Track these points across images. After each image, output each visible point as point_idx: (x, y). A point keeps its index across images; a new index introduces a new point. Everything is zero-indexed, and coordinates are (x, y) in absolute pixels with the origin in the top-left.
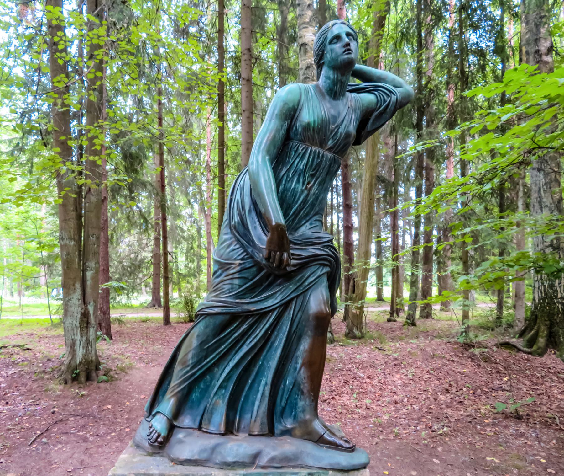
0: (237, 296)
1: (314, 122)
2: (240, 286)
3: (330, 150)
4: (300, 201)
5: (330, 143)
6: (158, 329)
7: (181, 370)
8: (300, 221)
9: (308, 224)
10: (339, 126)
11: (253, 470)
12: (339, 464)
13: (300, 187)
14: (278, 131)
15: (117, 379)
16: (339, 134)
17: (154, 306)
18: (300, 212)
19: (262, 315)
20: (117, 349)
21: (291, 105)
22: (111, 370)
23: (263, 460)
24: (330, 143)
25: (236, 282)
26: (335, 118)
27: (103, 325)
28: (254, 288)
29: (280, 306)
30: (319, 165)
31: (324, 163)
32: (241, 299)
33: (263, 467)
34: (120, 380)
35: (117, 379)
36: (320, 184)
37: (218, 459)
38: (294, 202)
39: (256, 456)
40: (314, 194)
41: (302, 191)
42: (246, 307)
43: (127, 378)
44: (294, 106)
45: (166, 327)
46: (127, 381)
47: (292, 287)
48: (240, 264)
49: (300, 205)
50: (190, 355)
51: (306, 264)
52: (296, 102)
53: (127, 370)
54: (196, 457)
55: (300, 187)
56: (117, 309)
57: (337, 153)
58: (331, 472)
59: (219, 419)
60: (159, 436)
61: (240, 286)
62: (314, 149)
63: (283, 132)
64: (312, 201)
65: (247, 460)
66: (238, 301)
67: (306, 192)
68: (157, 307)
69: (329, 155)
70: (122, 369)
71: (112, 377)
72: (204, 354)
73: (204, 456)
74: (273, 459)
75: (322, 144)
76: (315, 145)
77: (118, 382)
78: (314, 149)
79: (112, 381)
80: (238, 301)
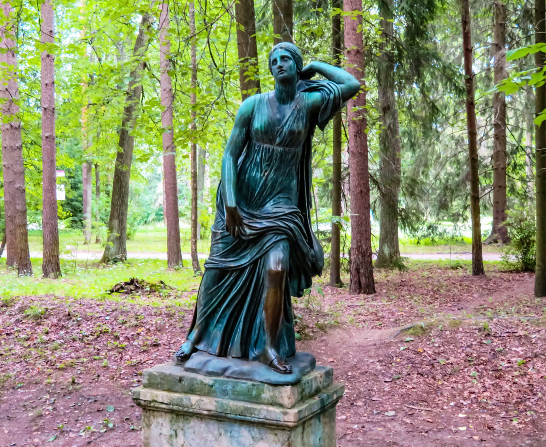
0: (222, 256)
1: (261, 127)
2: (224, 249)
3: (279, 145)
4: (260, 185)
5: (278, 140)
6: (462, 280)
7: (202, 310)
8: (265, 200)
9: (271, 201)
10: (283, 127)
11: (221, 378)
12: (269, 379)
13: (259, 175)
14: (238, 136)
15: (311, 338)
16: (284, 133)
17: (496, 242)
18: (263, 193)
19: (241, 270)
20: (371, 306)
21: (246, 116)
22: (308, 327)
23: (228, 373)
24: (278, 140)
25: (220, 245)
26: (280, 121)
27: (362, 271)
28: (235, 250)
29: (251, 264)
30: (271, 157)
31: (275, 157)
32: (225, 258)
33: (228, 377)
34: (315, 339)
35: (311, 338)
36: (276, 170)
37: (205, 369)
38: (256, 186)
39: (225, 370)
40: (271, 179)
41: (261, 178)
42: (228, 265)
43: (324, 338)
44: (248, 116)
45: (475, 278)
46: (323, 341)
47: (257, 250)
48: (221, 233)
49: (261, 187)
50: (201, 298)
51: (263, 233)
52: (250, 111)
53: (327, 330)
54: (194, 367)
55: (259, 175)
56: (438, 245)
57: (287, 146)
58: (266, 385)
59: (216, 346)
60: (183, 353)
61: (224, 249)
62: (265, 146)
63: (242, 136)
64: (272, 184)
65: (219, 371)
66: (223, 259)
67: (264, 178)
68: (500, 242)
69: (280, 149)
70: (322, 328)
71: (306, 335)
72: (210, 297)
73: (199, 367)
74: (233, 372)
75: (272, 141)
76: (266, 143)
77: (312, 341)
78: (265, 146)
79: (305, 339)
80: (223, 259)
